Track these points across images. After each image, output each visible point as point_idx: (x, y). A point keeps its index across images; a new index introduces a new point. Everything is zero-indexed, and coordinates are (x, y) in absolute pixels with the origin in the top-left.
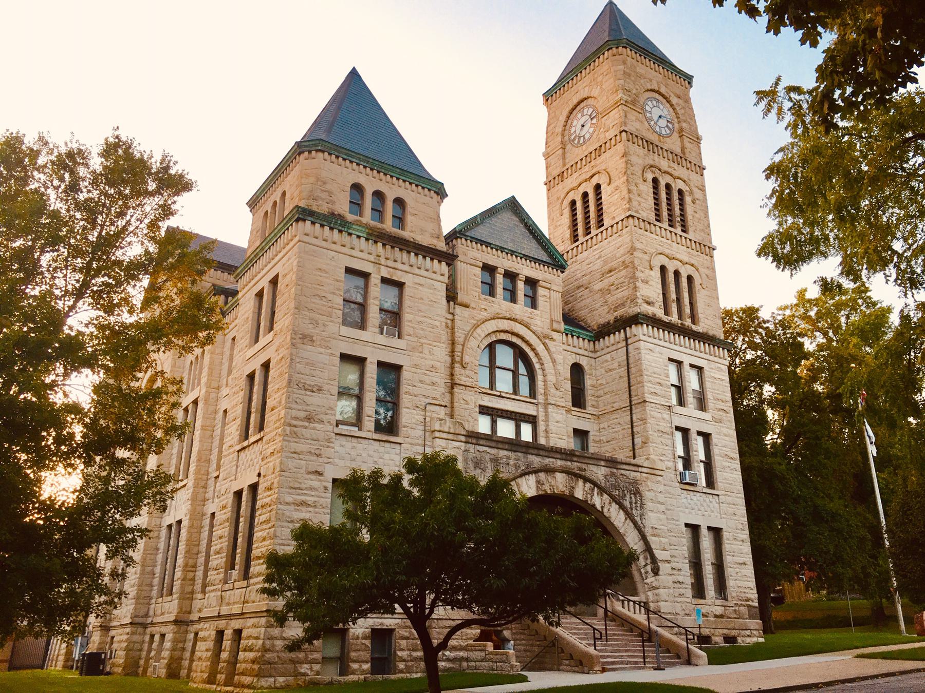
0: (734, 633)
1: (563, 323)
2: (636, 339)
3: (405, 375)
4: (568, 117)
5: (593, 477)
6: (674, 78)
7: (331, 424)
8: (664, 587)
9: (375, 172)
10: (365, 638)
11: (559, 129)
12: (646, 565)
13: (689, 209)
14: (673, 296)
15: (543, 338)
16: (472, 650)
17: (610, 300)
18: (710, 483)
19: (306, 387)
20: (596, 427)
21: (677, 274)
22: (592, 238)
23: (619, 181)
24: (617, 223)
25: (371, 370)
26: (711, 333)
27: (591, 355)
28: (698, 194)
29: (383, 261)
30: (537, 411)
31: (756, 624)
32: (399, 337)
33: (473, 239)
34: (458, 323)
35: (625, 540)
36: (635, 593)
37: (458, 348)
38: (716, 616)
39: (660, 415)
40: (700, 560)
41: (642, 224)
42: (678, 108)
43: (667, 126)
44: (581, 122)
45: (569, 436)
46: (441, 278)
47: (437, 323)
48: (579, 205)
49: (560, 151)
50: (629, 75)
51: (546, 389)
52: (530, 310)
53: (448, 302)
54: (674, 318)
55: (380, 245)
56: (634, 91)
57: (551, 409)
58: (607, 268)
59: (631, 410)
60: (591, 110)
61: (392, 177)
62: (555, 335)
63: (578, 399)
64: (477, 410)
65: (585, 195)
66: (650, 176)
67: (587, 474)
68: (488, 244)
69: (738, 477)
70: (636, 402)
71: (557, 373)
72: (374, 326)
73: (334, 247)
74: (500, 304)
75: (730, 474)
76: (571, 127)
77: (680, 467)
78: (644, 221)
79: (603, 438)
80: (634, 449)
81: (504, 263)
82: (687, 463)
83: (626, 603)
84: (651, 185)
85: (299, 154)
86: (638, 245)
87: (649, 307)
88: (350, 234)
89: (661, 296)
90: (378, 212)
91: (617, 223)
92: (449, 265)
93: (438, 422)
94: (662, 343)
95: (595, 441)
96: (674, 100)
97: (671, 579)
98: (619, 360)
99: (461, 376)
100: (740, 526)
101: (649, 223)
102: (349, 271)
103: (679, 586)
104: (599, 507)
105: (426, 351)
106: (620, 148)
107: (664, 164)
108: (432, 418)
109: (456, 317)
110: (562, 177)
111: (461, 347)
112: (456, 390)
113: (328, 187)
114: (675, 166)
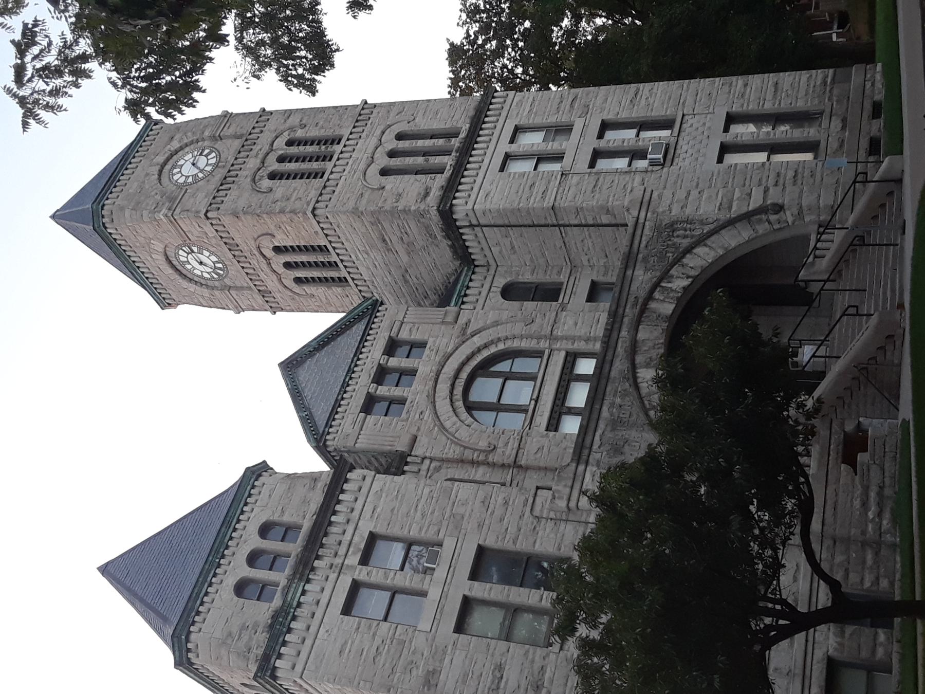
0: (868, 106)
1: (448, 308)
2: (471, 214)
3: (491, 542)
4: (191, 280)
5: (648, 287)
6: (151, 138)
7: (548, 655)
8: (800, 197)
9: (222, 561)
10: (842, 633)
11: (206, 292)
12: (770, 223)
13: (313, 133)
14: (420, 160)
15: (465, 336)
16: (868, 480)
17: (421, 243)
18: (666, 124)
19: (494, 687)
20: (588, 271)
21: (392, 154)
22: (342, 261)
23: (269, 224)
24: (322, 229)
25: (479, 590)
26: (472, 113)
27: (492, 272)
28: (294, 120)
29: (338, 561)
30: (559, 350)
31: (856, 71)
32: (440, 545)
33: (328, 425)
34: (436, 453)
35: (734, 249)
36: (807, 238)
37: (468, 454)
38: (844, 128)
39: (573, 189)
40: (768, 144)
41: (325, 197)
42: (186, 141)
43: (206, 156)
44: (196, 265)
45: (597, 310)
46: (368, 480)
47: (427, 490)
48: (301, 274)
49: (233, 292)
50: (138, 203)
51: (529, 337)
52: (427, 351)
53: (403, 473)
54: (448, 161)
55: (317, 563)
56: (158, 197)
57: (558, 332)
58: (380, 245)
59: (564, 226)
60: (181, 252)
61: (231, 538)
62: (462, 320)
63: (549, 293)
64: (551, 434)
65: (288, 265)
66: (266, 183)
67: (643, 294)
68: (337, 404)
69: (661, 87)
70: (554, 219)
71: (512, 319)
72: (423, 581)
73: (313, 629)
74: (415, 392)
75: (657, 97)
76: (202, 277)
77: (642, 164)
78: (321, 194)
79: (602, 262)
80: (617, 225)
81: (362, 384)
82: (637, 154)
83: (818, 252)
84: (277, 182)
85: (192, 664)
86: (351, 204)
87: (431, 194)
88: (299, 604)
89: (419, 177)
90: (274, 561)
91: (322, 229)
92: (352, 468)
93: (557, 501)
94: (479, 180)
95: (605, 274)
96: (175, 145)
97: (789, 188)
98: (499, 236)
99: (505, 454)
100: (726, 88)
101: (325, 187)
102: (347, 610)
103: (800, 176)
104: (686, 283)
105: (461, 510)
106: (227, 220)
107: (253, 163)
108: (551, 510)
109: (428, 455)
110: (265, 292)
111: (467, 451)
112: (523, 463)
113: (235, 630)
114: (256, 148)
